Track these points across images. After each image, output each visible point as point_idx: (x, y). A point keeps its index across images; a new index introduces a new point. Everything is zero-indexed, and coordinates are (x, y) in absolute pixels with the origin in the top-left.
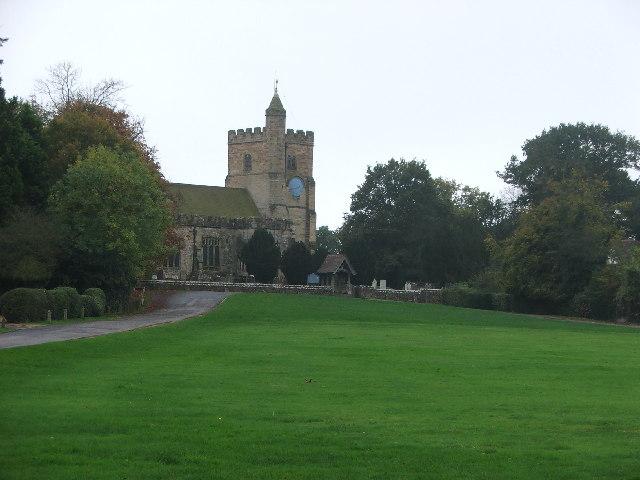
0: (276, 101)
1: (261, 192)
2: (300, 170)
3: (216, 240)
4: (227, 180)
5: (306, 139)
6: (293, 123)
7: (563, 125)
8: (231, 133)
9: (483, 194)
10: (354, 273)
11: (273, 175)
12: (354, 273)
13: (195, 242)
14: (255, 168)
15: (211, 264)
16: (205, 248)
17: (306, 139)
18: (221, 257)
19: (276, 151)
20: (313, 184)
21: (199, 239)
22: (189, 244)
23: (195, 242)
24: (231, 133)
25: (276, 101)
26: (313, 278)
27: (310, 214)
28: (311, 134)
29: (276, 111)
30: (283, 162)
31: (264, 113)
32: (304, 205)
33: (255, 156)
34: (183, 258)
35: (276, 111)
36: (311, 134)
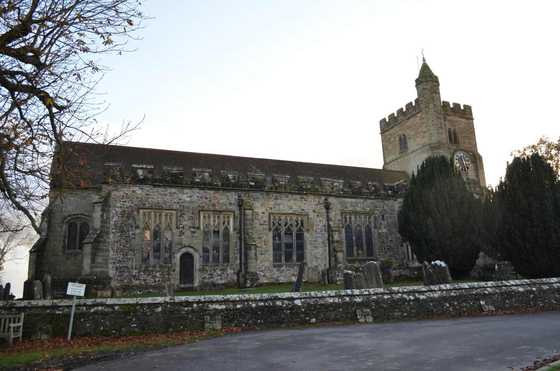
5: (465, 113)
13: (328, 220)
17: (465, 113)
20: (480, 158)
21: (335, 214)
22: (319, 223)
28: (468, 109)
29: (427, 80)
35: (427, 80)
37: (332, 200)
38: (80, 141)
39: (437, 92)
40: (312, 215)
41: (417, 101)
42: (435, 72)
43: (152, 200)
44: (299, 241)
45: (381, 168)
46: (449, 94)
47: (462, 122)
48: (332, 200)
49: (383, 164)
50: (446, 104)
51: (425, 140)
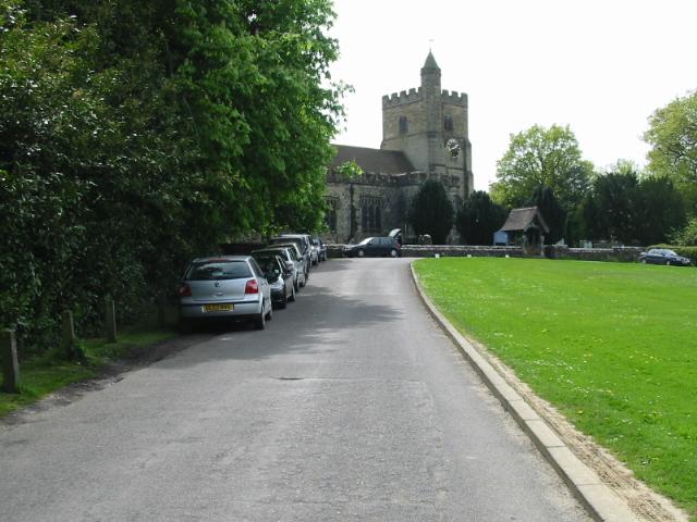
0: (430, 59)
1: (418, 152)
2: (457, 132)
3: (378, 200)
4: (383, 144)
5: (461, 101)
6: (448, 84)
7: (499, 163)
8: (385, 98)
9: (584, 163)
10: (547, 230)
11: (431, 134)
12: (547, 230)
13: (352, 201)
14: (411, 129)
15: (371, 225)
16: (364, 208)
17: (461, 101)
18: (383, 220)
19: (431, 112)
20: (470, 145)
21: (356, 198)
22: (346, 203)
23: (352, 201)
24: (385, 98)
25: (430, 59)
26: (500, 237)
27: (468, 176)
28: (465, 96)
29: (431, 71)
30: (440, 121)
31: (419, 72)
32: (461, 166)
33: (410, 117)
34: (339, 220)
35: (431, 71)
36: (465, 96)
37: (355, 187)
38: (527, 422)
39: (439, 84)
40: (342, 197)
41: (420, 89)
42: (439, 65)
43: (144, 11)
44: (361, 253)
45: (379, 148)
46: (448, 84)
47: (458, 110)
48: (355, 187)
49: (382, 139)
50: (446, 92)
51: (424, 128)
